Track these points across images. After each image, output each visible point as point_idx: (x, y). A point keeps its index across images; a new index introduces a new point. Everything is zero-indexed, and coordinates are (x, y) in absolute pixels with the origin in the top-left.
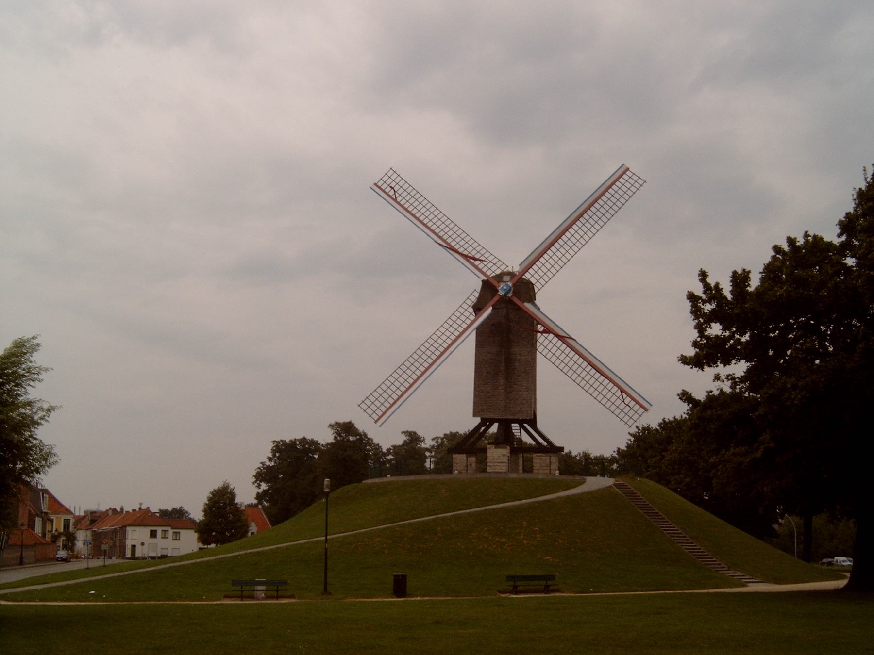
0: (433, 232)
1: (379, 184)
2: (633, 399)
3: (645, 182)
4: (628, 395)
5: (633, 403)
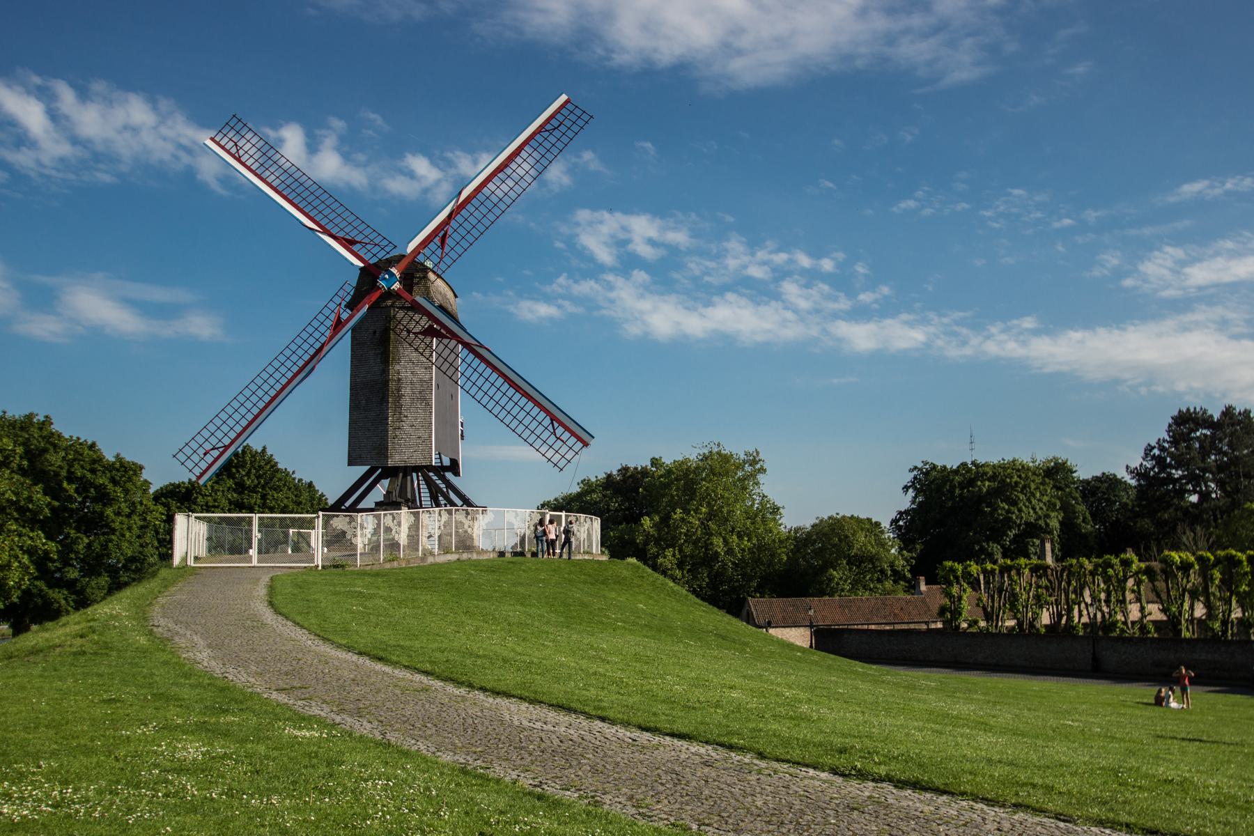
0: (290, 381)
1: (580, 445)
2: (567, 429)
3: (591, 117)
4: (561, 424)
5: (567, 435)
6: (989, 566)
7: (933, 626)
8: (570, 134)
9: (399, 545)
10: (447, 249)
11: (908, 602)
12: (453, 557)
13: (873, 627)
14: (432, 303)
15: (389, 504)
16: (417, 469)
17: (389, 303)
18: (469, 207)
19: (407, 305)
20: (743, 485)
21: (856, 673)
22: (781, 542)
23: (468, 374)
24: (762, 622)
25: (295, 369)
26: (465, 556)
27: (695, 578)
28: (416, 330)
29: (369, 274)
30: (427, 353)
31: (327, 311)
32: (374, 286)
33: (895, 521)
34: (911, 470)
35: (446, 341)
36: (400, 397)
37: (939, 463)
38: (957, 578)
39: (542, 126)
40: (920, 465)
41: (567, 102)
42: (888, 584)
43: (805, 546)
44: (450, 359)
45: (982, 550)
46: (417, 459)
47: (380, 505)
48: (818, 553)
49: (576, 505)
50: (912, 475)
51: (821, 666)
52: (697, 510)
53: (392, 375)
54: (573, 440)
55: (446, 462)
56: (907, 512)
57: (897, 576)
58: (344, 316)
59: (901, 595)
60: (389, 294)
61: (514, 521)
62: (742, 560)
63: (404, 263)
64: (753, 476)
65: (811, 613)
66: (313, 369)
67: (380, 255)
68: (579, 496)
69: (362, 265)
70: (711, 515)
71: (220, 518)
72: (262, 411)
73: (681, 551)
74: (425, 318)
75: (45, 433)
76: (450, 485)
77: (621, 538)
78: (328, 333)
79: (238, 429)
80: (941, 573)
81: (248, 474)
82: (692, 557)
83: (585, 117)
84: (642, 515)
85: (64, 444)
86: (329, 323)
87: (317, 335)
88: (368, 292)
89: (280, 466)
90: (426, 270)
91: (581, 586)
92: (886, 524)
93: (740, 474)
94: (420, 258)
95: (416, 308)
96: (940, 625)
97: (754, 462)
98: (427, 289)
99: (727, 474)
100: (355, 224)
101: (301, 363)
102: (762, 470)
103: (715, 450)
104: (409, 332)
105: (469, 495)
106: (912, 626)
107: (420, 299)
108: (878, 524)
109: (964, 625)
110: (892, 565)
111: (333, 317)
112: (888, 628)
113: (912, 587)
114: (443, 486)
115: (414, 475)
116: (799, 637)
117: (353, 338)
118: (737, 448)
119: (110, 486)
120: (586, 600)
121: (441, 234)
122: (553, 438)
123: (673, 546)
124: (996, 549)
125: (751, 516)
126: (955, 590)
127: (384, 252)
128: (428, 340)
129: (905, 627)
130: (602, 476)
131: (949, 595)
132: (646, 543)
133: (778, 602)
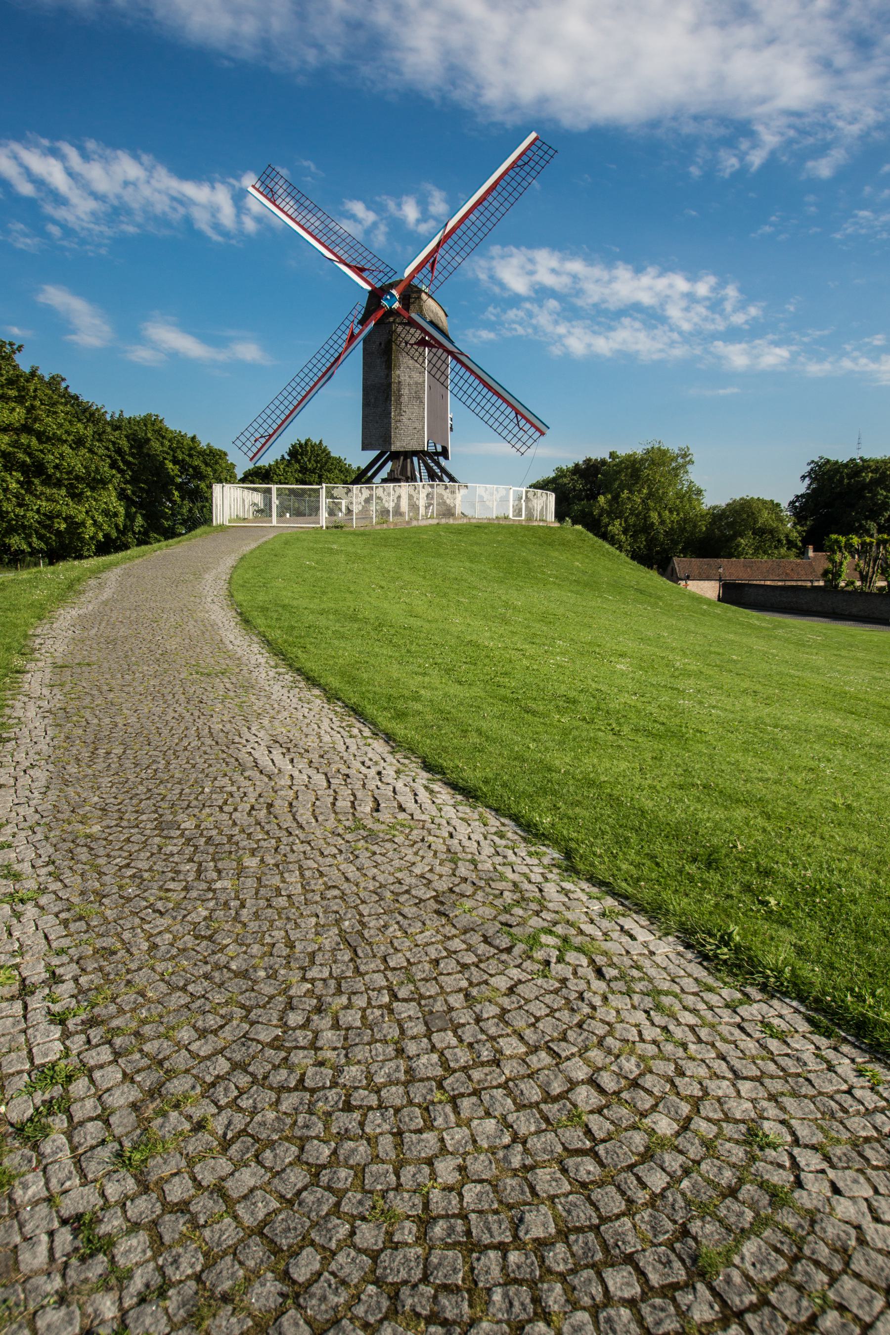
1: (538, 434)
2: (528, 421)
4: (524, 417)
6: (868, 540)
7: (816, 584)
8: (538, 168)
9: (388, 511)
10: (436, 273)
11: (798, 565)
12: (435, 522)
13: (768, 583)
14: (424, 319)
15: (391, 479)
16: (415, 453)
17: (391, 319)
18: (454, 236)
19: (405, 321)
20: (675, 473)
21: (751, 626)
22: (702, 516)
23: (456, 381)
24: (683, 576)
25: (320, 374)
26: (443, 521)
27: (635, 541)
28: (412, 342)
29: (376, 295)
30: (421, 359)
31: (343, 328)
32: (379, 306)
33: (792, 503)
34: (809, 464)
35: (434, 350)
36: (400, 396)
37: (833, 458)
38: (840, 548)
39: (514, 162)
40: (816, 459)
41: (536, 139)
42: (783, 551)
43: (721, 519)
44: (442, 369)
45: (861, 526)
46: (413, 446)
47: (384, 481)
48: (731, 525)
49: (551, 486)
50: (809, 468)
51: (722, 620)
52: (639, 491)
53: (394, 379)
54: (533, 430)
55: (439, 449)
56: (802, 496)
57: (791, 544)
58: (356, 331)
59: (792, 559)
60: (391, 312)
61: (483, 494)
62: (672, 529)
63: (402, 286)
64: (683, 466)
65: (721, 570)
66: (333, 373)
67: (384, 280)
68: (554, 480)
69: (369, 288)
70: (650, 495)
71: (289, 489)
72: (296, 407)
73: (626, 521)
74: (419, 332)
75: (156, 428)
76: (443, 470)
77: (582, 511)
78: (344, 345)
79: (279, 422)
80: (827, 544)
81: (309, 460)
82: (634, 526)
83: (551, 152)
84: (599, 494)
85: (170, 436)
86: (345, 337)
87: (336, 346)
88: (375, 311)
89: (332, 455)
90: (420, 291)
91: (530, 546)
92: (784, 505)
93: (674, 465)
94: (415, 282)
95: (412, 323)
96: (822, 583)
97: (685, 456)
98: (421, 308)
99: (664, 464)
100: (365, 254)
101: (324, 370)
102: (691, 462)
103: (657, 446)
104: (406, 343)
105: (454, 474)
106: (800, 583)
107: (414, 316)
108: (778, 505)
109: (842, 584)
110: (787, 536)
111: (348, 332)
112: (780, 584)
113: (802, 553)
114: (438, 471)
115: (415, 459)
116: (709, 589)
117: (365, 349)
118: (672, 446)
119: (203, 467)
120: (530, 558)
121: (431, 260)
122: (517, 429)
123: (620, 518)
124: (872, 526)
125: (680, 496)
126: (838, 557)
127: (386, 278)
128: (421, 349)
129: (794, 583)
130: (571, 465)
131: (832, 561)
132: (601, 515)
133: (696, 561)
